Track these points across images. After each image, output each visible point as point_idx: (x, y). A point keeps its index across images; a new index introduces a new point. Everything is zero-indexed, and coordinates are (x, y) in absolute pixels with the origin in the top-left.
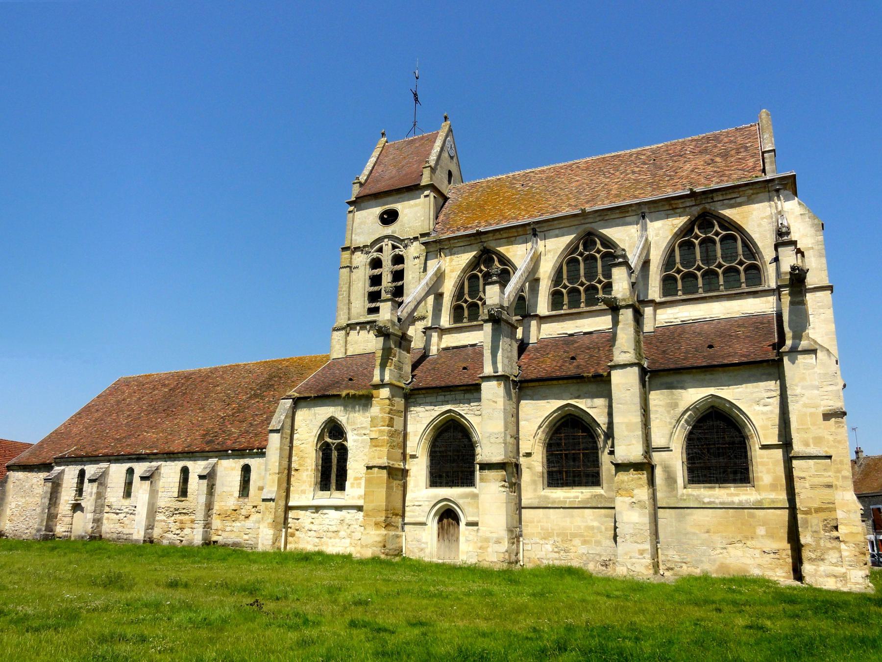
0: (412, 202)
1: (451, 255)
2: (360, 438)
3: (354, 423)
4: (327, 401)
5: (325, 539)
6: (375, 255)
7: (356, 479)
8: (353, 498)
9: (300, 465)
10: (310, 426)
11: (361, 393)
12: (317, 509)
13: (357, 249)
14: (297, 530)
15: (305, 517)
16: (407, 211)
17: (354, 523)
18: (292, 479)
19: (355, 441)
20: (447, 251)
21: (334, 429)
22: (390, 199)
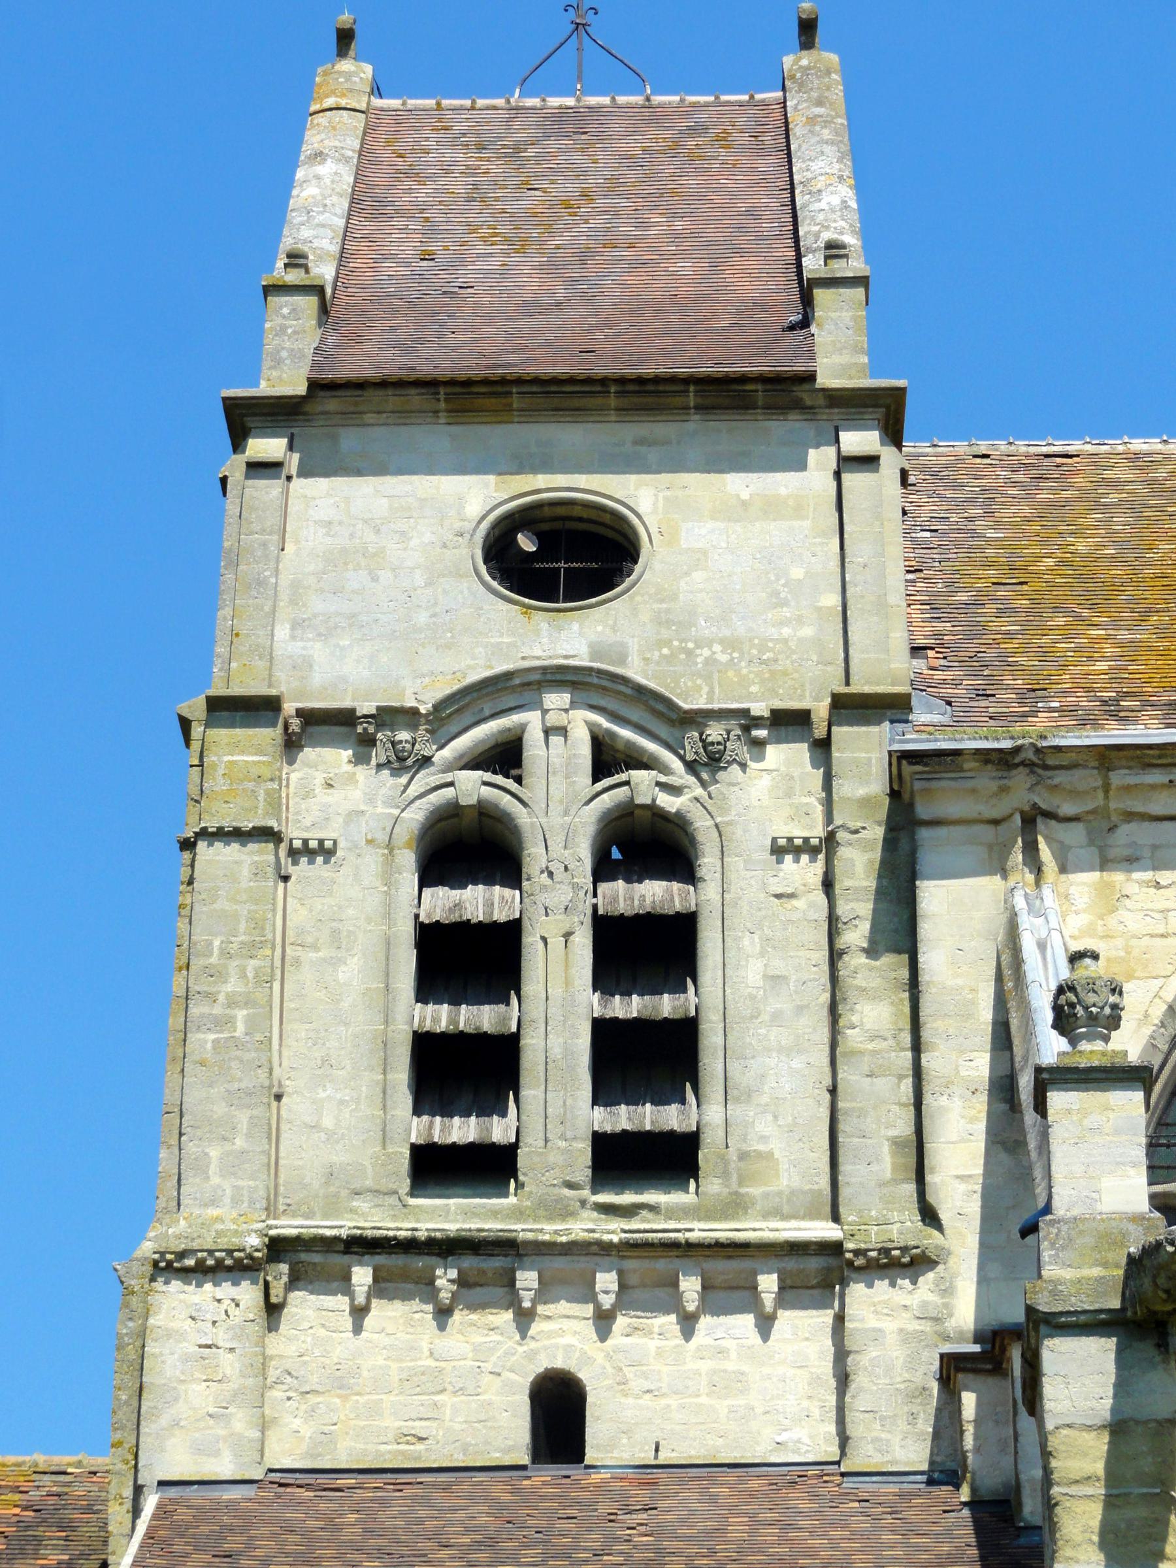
0: (740, 485)
1: (1105, 863)
6: (472, 786)
13: (330, 723)
16: (699, 533)
20: (1074, 834)
22: (570, 435)
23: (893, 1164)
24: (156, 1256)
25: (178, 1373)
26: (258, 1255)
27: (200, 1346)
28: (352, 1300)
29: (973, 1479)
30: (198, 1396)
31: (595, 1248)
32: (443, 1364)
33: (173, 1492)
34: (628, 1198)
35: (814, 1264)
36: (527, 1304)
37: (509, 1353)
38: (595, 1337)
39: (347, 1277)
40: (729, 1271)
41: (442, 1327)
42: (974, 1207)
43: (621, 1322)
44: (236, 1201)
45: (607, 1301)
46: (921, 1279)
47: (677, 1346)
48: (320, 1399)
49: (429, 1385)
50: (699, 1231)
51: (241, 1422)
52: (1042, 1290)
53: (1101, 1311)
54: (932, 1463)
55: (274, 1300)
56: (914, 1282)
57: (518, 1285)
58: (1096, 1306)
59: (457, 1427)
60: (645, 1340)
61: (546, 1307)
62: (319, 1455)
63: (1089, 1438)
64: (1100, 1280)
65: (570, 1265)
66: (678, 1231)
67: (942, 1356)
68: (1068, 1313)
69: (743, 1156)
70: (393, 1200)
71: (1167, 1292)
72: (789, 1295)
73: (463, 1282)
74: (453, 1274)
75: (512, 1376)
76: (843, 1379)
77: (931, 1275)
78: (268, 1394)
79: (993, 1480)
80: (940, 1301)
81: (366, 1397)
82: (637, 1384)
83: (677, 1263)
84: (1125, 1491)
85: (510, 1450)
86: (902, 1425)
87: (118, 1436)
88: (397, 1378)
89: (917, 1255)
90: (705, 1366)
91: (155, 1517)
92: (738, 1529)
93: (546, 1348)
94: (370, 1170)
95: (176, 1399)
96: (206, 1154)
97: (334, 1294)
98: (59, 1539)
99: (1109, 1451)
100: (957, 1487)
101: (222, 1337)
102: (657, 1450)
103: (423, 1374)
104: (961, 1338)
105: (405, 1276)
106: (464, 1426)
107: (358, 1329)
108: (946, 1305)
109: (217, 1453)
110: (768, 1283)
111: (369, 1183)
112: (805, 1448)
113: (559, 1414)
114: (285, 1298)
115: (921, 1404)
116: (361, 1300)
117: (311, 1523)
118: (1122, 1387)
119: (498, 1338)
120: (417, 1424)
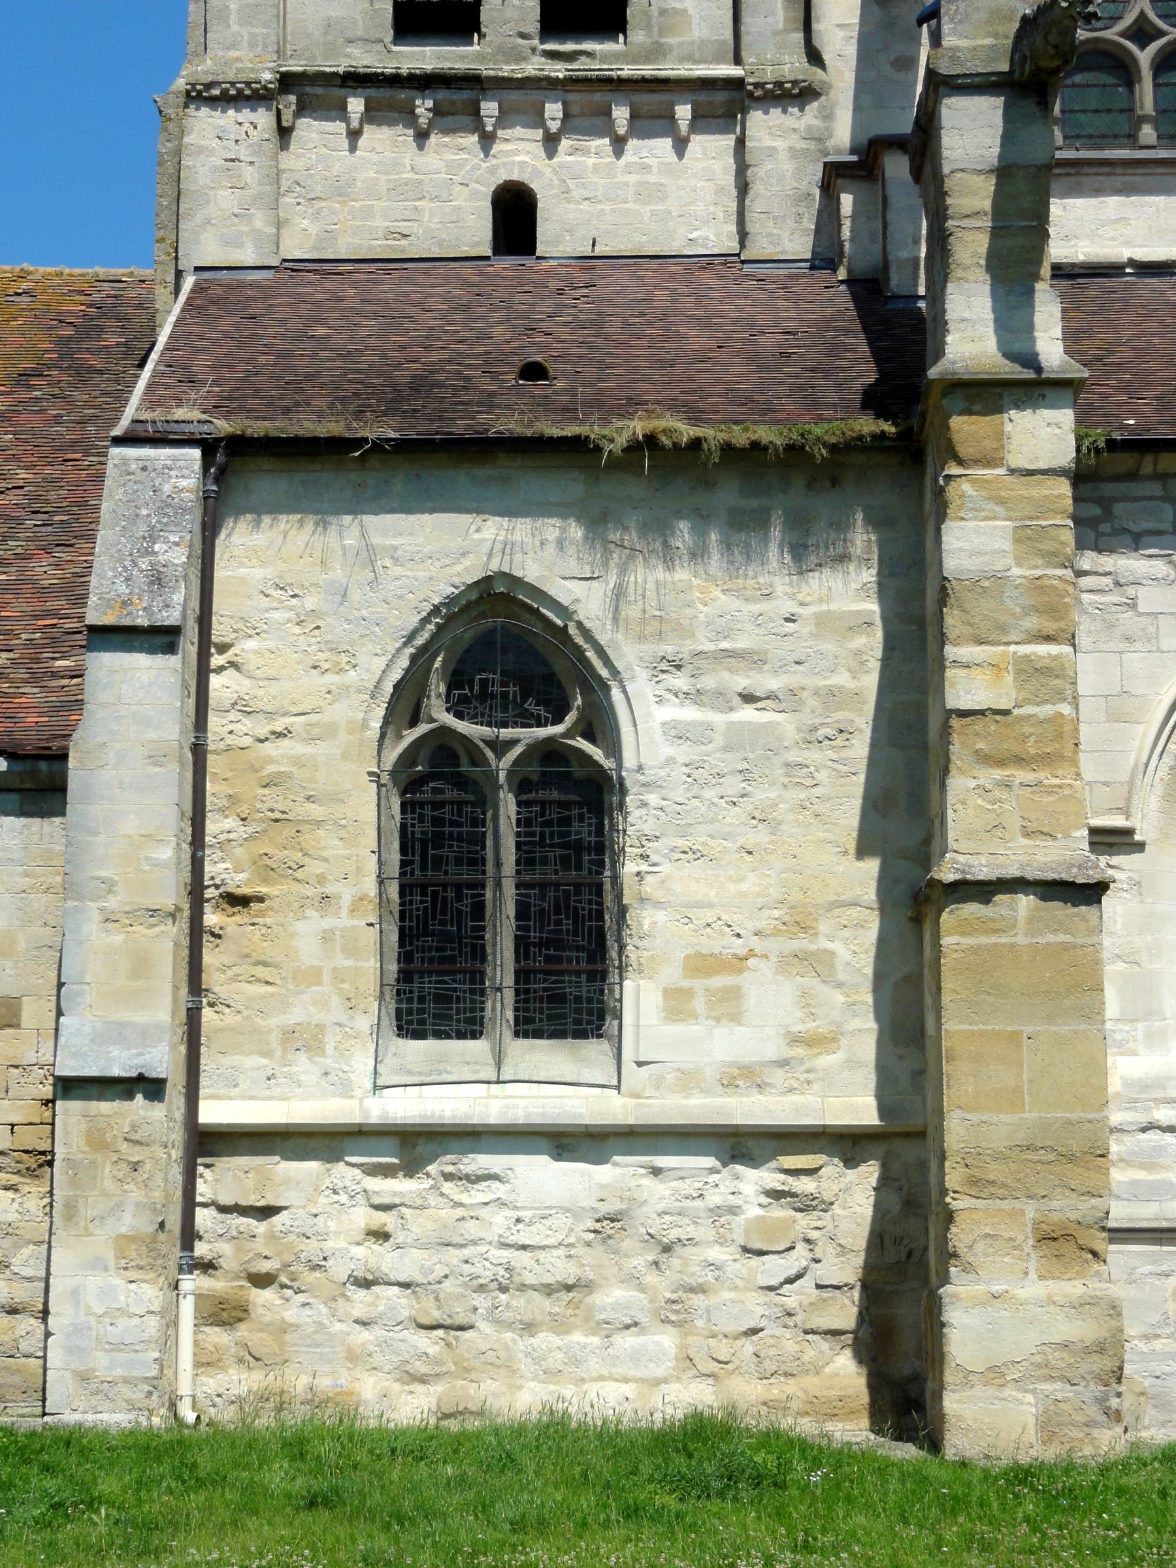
2: (717, 718)
3: (659, 626)
4: (462, 478)
5: (484, 1335)
7: (703, 964)
8: (688, 1080)
9: (266, 869)
10: (337, 629)
11: (740, 437)
12: (414, 1145)
14: (262, 1280)
15: (326, 1204)
17: (704, 1232)
18: (209, 958)
19: (678, 733)
21: (503, 654)
23: (785, 17)
24: (189, 87)
25: (208, 181)
26: (272, 86)
27: (226, 160)
28: (348, 125)
29: (849, 263)
30: (225, 200)
31: (544, 83)
32: (422, 177)
33: (207, 275)
34: (569, 47)
35: (720, 97)
36: (489, 128)
37: (475, 168)
38: (544, 155)
39: (343, 107)
40: (652, 102)
41: (421, 147)
42: (852, 50)
43: (565, 143)
44: (252, 45)
45: (554, 126)
46: (807, 108)
47: (610, 163)
48: (323, 204)
49: (406, 194)
50: (628, 71)
51: (260, 221)
52: (943, 56)
53: (993, 74)
54: (814, 253)
55: (285, 124)
56: (802, 110)
57: (482, 113)
58: (989, 70)
59: (434, 226)
60: (584, 158)
61: (505, 132)
62: (324, 248)
63: (979, 180)
64: (991, 47)
65: (522, 96)
66: (612, 70)
67: (825, 164)
68: (965, 75)
69: (663, 12)
70: (380, 47)
71: (1056, 47)
72: (699, 123)
73: (437, 111)
74: (430, 103)
75: (478, 186)
76: (743, 188)
77: (815, 104)
78: (281, 200)
79: (868, 261)
80: (823, 125)
81: (361, 203)
82: (577, 193)
83: (609, 96)
84: (1008, 224)
85: (477, 244)
86: (790, 223)
87: (161, 233)
88: (385, 188)
89: (804, 87)
90: (633, 178)
91: (192, 291)
92: (661, 297)
93: (504, 164)
94: (360, 23)
95: (208, 202)
96: (227, 7)
97: (333, 120)
98: (117, 327)
99: (995, 190)
100: (835, 270)
101: (243, 152)
102: (594, 245)
103: (406, 184)
104: (839, 152)
105: (391, 106)
106: (440, 226)
107: (353, 148)
108: (827, 129)
109: (241, 245)
110: (684, 112)
111: (360, 33)
112: (712, 244)
113: (515, 214)
114: (294, 123)
115: (806, 207)
116: (355, 124)
117: (320, 296)
118: (1007, 138)
119: (464, 156)
120: (402, 224)
